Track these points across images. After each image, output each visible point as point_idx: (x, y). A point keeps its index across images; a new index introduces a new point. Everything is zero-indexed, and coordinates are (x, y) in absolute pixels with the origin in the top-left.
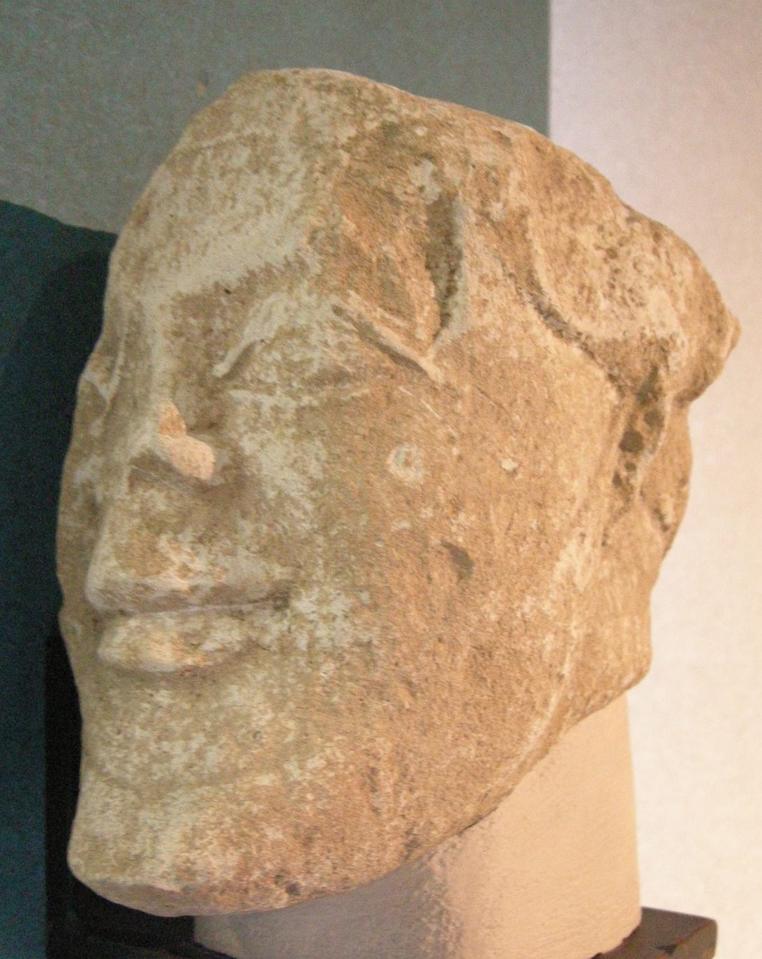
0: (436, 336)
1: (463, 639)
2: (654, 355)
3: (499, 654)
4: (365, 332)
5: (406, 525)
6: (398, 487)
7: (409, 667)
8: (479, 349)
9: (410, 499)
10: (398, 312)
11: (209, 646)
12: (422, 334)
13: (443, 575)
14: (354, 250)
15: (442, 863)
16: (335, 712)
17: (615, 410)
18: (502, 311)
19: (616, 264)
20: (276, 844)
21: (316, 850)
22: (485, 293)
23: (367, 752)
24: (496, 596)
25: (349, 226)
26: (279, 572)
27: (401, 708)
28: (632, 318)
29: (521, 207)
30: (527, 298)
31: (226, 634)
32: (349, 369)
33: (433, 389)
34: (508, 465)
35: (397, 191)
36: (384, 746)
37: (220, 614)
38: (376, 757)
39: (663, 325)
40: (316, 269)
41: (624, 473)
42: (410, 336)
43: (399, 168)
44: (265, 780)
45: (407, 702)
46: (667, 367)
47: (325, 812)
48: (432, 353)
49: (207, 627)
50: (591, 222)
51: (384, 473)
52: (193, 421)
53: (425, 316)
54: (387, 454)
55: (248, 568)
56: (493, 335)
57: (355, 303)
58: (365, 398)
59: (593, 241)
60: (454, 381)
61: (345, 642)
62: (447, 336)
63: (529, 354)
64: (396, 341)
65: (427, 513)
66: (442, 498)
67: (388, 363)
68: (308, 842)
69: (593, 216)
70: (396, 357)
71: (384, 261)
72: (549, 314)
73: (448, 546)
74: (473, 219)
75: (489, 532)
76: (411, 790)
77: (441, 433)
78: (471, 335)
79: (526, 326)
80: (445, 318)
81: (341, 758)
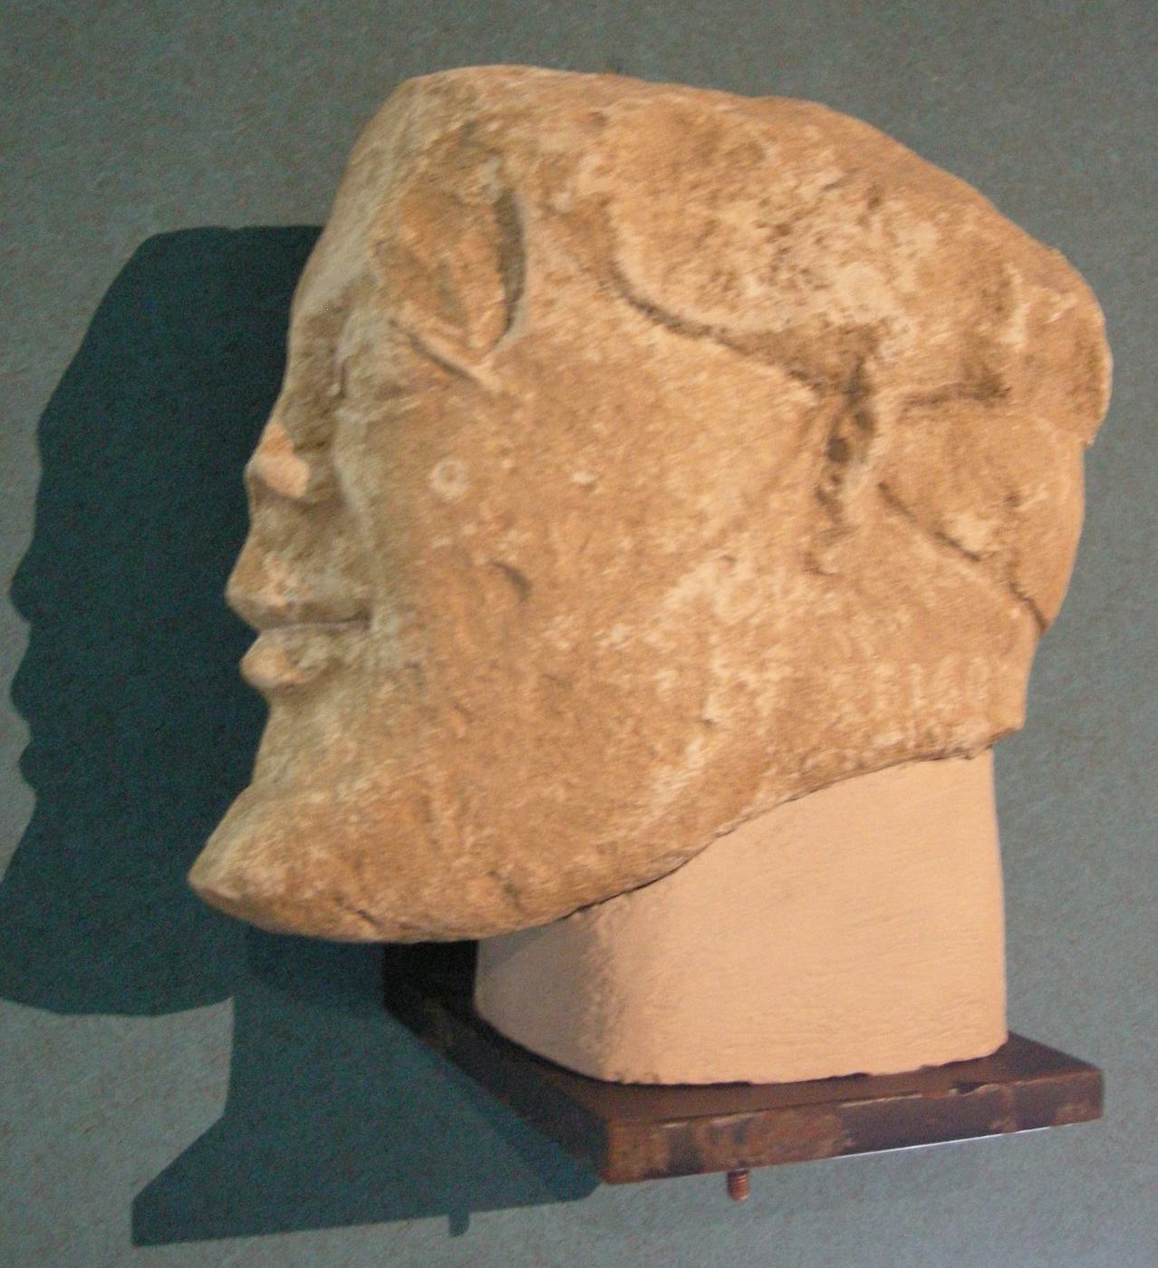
0: (496, 342)
1: (522, 664)
4: (416, 344)
5: (445, 541)
6: (439, 503)
7: (459, 693)
8: (543, 354)
9: (452, 514)
10: (450, 320)
11: (305, 663)
12: (478, 342)
13: (498, 598)
14: (413, 261)
15: (609, 924)
16: (389, 734)
17: (806, 419)
18: (576, 311)
19: (785, 241)
20: (320, 863)
21: (369, 875)
22: (552, 293)
23: (416, 779)
24: (563, 622)
25: (408, 234)
26: (359, 590)
31: (318, 651)
32: (403, 382)
33: (487, 399)
34: (581, 478)
35: (462, 192)
36: (437, 776)
37: (319, 633)
38: (426, 784)
39: (864, 308)
40: (381, 283)
41: (828, 488)
42: (463, 344)
43: (467, 169)
44: (318, 798)
45: (462, 731)
47: (368, 836)
48: (488, 362)
49: (305, 646)
50: (750, 197)
52: (300, 440)
53: (483, 322)
54: (431, 467)
55: (333, 586)
56: (560, 338)
57: (409, 313)
58: (415, 411)
59: (753, 218)
60: (514, 389)
61: (398, 664)
62: (509, 340)
63: (618, 353)
64: (444, 349)
65: (469, 529)
67: (439, 374)
68: (358, 866)
69: (753, 188)
70: (448, 368)
71: (443, 267)
72: (650, 310)
73: (499, 565)
74: (537, 214)
75: (550, 552)
77: (491, 445)
78: (532, 338)
79: (614, 324)
80: (509, 322)
81: (386, 782)
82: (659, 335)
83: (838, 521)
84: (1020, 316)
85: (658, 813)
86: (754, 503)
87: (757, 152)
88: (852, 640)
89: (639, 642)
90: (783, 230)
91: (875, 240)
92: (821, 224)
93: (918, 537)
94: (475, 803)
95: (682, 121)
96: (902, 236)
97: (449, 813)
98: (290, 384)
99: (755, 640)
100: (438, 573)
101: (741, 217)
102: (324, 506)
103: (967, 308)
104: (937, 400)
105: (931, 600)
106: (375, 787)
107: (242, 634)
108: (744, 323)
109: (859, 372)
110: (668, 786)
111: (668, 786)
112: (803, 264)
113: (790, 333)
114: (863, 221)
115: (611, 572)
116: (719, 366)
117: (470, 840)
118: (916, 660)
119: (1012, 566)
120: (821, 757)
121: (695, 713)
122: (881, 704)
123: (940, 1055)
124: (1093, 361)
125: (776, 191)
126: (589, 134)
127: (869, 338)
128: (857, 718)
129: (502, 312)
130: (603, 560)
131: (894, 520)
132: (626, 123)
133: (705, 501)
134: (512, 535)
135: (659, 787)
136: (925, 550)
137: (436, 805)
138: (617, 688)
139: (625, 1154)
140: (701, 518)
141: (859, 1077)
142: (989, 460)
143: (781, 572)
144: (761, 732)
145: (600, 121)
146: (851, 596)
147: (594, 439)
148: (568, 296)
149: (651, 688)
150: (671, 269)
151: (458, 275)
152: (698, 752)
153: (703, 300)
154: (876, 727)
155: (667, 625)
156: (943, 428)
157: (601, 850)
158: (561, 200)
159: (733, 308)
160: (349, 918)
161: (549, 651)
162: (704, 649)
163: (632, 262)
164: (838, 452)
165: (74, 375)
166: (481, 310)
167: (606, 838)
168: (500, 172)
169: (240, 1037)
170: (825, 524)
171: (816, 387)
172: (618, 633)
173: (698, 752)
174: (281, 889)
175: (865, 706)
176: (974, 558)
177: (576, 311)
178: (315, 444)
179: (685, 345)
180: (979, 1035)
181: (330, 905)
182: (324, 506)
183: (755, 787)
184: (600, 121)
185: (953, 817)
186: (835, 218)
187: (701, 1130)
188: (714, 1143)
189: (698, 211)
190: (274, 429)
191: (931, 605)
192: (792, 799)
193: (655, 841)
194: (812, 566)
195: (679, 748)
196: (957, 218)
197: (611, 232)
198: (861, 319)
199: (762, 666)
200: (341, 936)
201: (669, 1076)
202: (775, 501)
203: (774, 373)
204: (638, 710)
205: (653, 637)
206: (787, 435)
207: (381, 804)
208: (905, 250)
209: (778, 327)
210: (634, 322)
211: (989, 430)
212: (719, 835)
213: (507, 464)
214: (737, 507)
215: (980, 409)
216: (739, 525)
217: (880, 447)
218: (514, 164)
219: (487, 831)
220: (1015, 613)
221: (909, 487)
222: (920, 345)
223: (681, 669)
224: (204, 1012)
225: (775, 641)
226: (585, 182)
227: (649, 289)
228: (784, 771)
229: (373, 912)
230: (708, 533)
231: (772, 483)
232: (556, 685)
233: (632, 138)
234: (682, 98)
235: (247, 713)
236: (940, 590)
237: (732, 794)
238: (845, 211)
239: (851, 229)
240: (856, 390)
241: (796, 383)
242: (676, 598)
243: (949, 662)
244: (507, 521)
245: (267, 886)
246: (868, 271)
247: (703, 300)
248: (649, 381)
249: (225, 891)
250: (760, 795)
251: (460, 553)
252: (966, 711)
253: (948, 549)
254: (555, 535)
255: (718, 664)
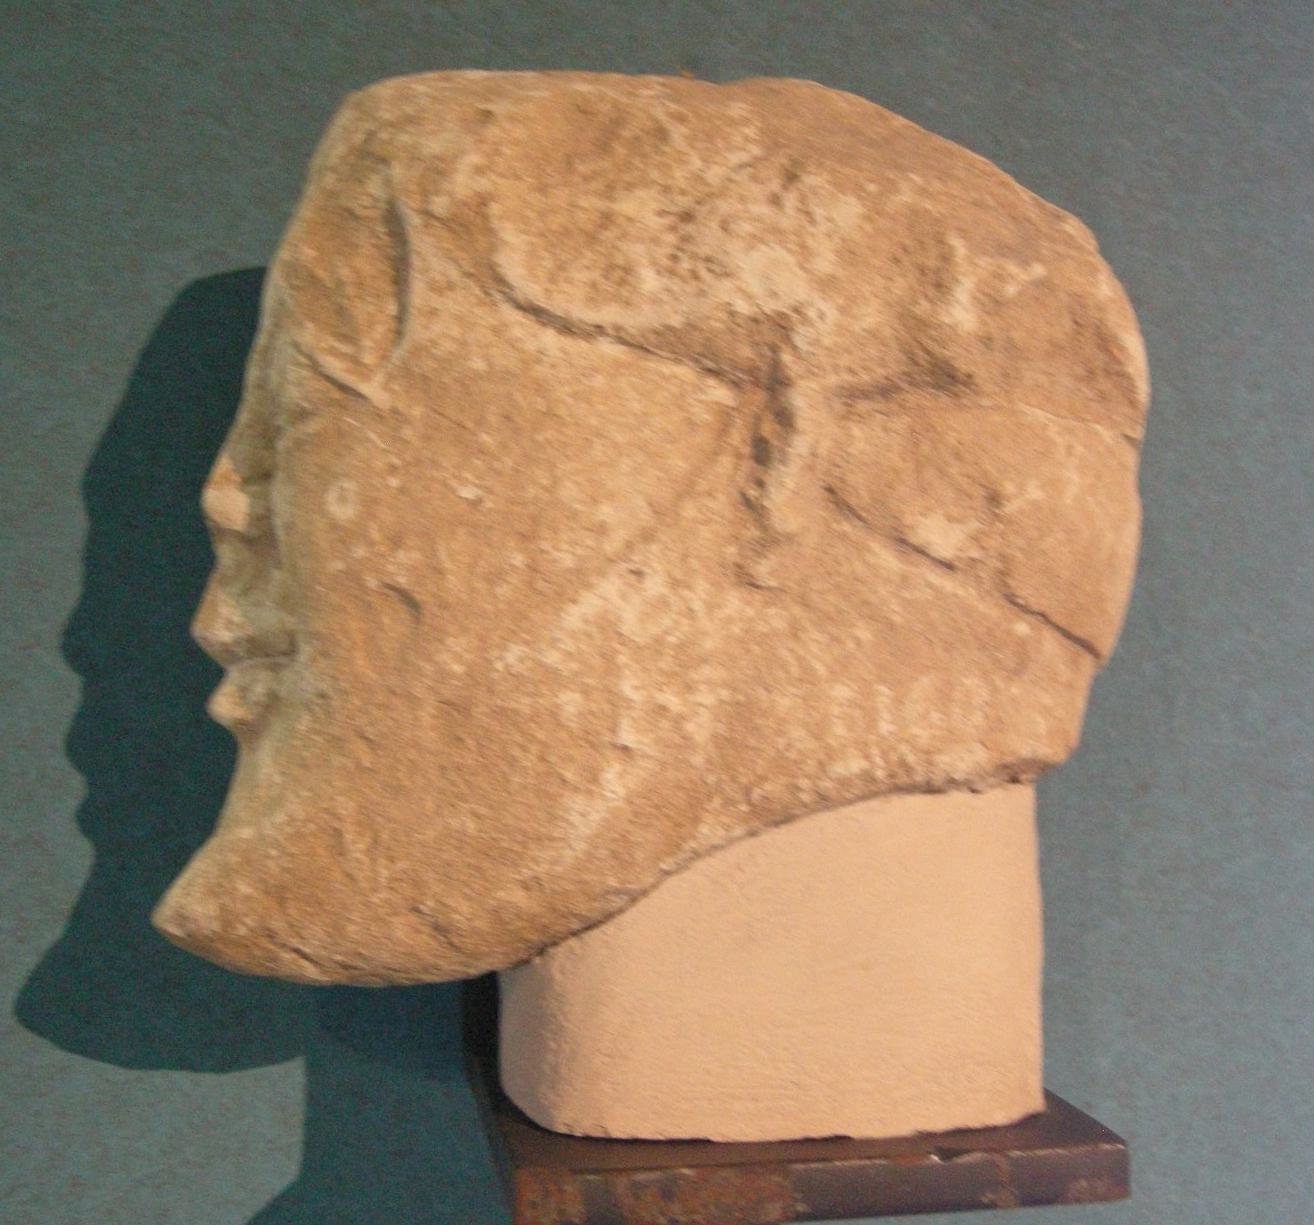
1: (419, 691)
2: (769, 334)
3: (479, 711)
4: (315, 367)
6: (334, 526)
8: (428, 365)
9: (345, 535)
13: (394, 622)
14: (314, 280)
17: (725, 416)
19: (690, 228)
20: (248, 898)
22: (436, 301)
23: (326, 811)
24: (457, 643)
27: (358, 765)
28: (702, 293)
29: (479, 195)
30: (498, 296)
33: (379, 416)
34: (468, 493)
36: (346, 806)
38: (339, 818)
39: (774, 294)
42: (355, 361)
46: (795, 348)
47: (287, 870)
48: (379, 378)
51: (323, 513)
55: (271, 619)
56: (447, 346)
59: (654, 206)
60: (400, 406)
62: (398, 354)
63: (505, 359)
64: (335, 367)
65: (360, 552)
66: (376, 535)
67: (337, 394)
68: (282, 901)
70: (343, 388)
71: (340, 284)
75: (439, 571)
76: (392, 860)
77: (379, 464)
80: (399, 334)
81: (301, 815)
82: (550, 338)
83: (764, 528)
84: (964, 291)
85: (581, 847)
86: (664, 513)
87: (662, 134)
88: (800, 659)
89: (541, 664)
90: (687, 217)
91: (789, 217)
92: (724, 206)
93: (875, 546)
94: (385, 836)
95: (584, 110)
96: (819, 212)
97: (362, 846)
98: (244, 417)
99: (681, 663)
100: (334, 598)
101: (641, 207)
102: (261, 538)
103: (900, 287)
104: (886, 391)
105: (897, 614)
106: (292, 820)
107: (208, 672)
108: (635, 321)
109: (776, 365)
110: (585, 818)
111: (585, 818)
112: (704, 251)
113: (691, 326)
114: (775, 201)
115: (503, 590)
116: (618, 366)
117: (385, 873)
118: (884, 682)
119: (1003, 575)
120: (768, 787)
121: (607, 738)
122: (839, 730)
123: (940, 1120)
124: (1106, 342)
125: (679, 176)
126: (460, 134)
127: (782, 325)
128: (810, 744)
129: (393, 325)
130: (495, 577)
131: (846, 527)
132: (512, 118)
133: (606, 512)
134: (402, 556)
135: (575, 818)
136: (887, 559)
137: (348, 837)
138: (516, 712)
139: (534, 1205)
140: (601, 530)
141: (840, 1140)
142: (958, 456)
143: (702, 586)
144: (698, 760)
145: (487, 116)
146: (797, 611)
147: (482, 451)
148: (450, 304)
149: (554, 713)
150: (561, 267)
151: (350, 291)
152: (616, 782)
153: (595, 296)
154: (831, 754)
155: (569, 645)
156: (900, 423)
157: (525, 886)
158: (440, 205)
159: (628, 303)
160: (287, 956)
161: (443, 674)
162: (611, 668)
163: (513, 265)
164: (762, 453)
165: (116, 429)
166: (371, 324)
167: (526, 873)
168: (388, 182)
169: (312, 1099)
170: (754, 532)
171: (736, 385)
172: (514, 654)
173: (616, 782)
174: (216, 926)
175: (818, 732)
176: (948, 566)
177: (459, 319)
178: (259, 476)
179: (576, 346)
180: (1036, 1103)
181: (265, 942)
182: (261, 538)
183: (696, 820)
184: (487, 116)
185: (988, 856)
186: (742, 199)
187: (621, 1184)
188: (637, 1197)
189: (591, 203)
190: (224, 465)
191: (897, 619)
192: (753, 834)
193: (587, 877)
194: (746, 580)
195: (593, 776)
196: (890, 187)
197: (490, 232)
198: (770, 306)
199: (689, 688)
200: (288, 977)
201: (617, 1132)
202: (689, 510)
203: (685, 372)
204: (541, 735)
205: (552, 658)
206: (704, 439)
207: (298, 836)
208: (824, 227)
209: (676, 321)
210: (520, 325)
211: (956, 424)
212: (667, 873)
213: (394, 482)
214: (645, 517)
215: (944, 399)
216: (648, 536)
217: (800, 446)
218: (397, 171)
219: (400, 865)
220: (1022, 628)
221: (859, 487)
222: (841, 330)
223: (586, 692)
224: (274, 1071)
225: (704, 660)
226: (463, 183)
227: (531, 290)
228: (729, 802)
229: (307, 950)
230: (612, 545)
231: (687, 489)
232: (455, 709)
233: (519, 132)
234: (582, 85)
235: (216, 756)
236: (908, 603)
237: (672, 824)
238: (756, 190)
239: (763, 210)
240: (776, 383)
241: (712, 382)
242: (574, 617)
243: (924, 685)
244: (396, 541)
245: (203, 923)
246: (780, 253)
247: (595, 296)
248: (540, 388)
249: (173, 929)
250: (704, 829)
251: (353, 576)
252: (952, 737)
253: (915, 556)
254: (443, 555)
255: (628, 687)
